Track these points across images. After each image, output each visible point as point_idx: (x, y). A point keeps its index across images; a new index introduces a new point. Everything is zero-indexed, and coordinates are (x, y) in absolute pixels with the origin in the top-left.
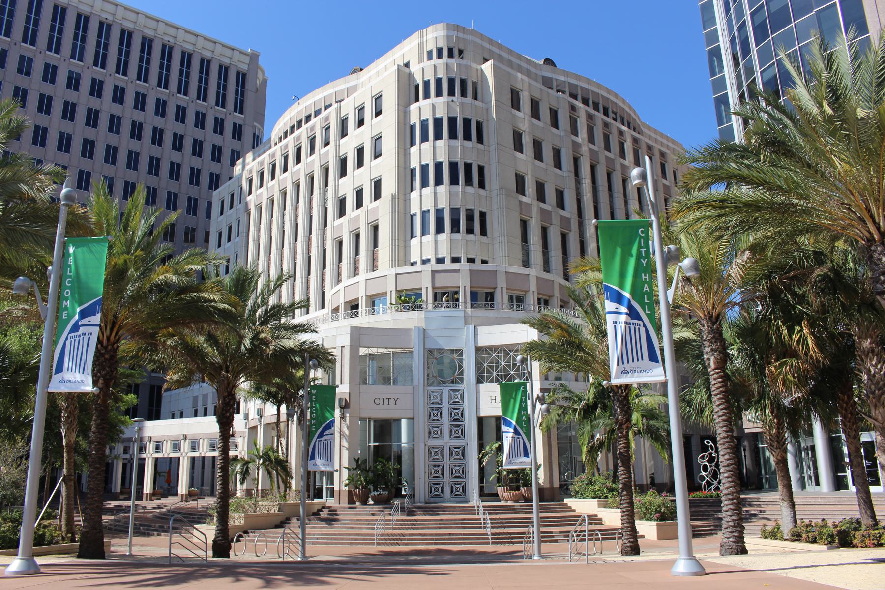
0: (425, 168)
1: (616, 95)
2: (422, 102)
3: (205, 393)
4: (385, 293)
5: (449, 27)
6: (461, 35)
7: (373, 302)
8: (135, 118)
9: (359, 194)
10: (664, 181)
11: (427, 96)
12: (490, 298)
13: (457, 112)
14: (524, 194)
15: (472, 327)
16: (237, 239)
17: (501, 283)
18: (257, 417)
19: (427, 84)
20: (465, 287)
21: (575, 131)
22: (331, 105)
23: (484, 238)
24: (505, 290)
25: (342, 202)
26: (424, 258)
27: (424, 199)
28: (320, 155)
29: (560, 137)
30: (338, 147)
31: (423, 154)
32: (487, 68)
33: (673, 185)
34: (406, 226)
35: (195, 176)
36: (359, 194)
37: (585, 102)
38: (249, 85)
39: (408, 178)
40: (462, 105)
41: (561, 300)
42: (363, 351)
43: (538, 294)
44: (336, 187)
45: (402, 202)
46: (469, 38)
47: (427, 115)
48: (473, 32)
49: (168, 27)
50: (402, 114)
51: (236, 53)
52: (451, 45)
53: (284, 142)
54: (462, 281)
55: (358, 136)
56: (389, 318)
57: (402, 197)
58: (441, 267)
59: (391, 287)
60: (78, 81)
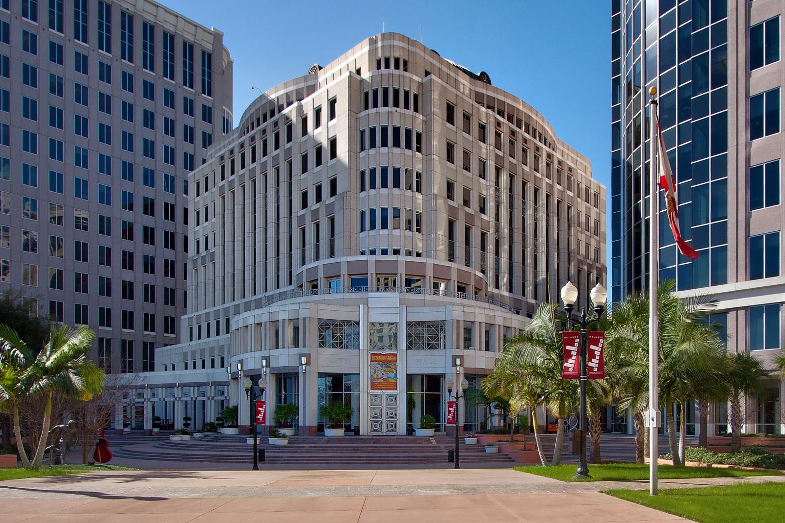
2: (372, 111)
7: (330, 283)
16: (214, 220)
35: (170, 155)
37: (510, 119)
41: (476, 288)
59: (344, 271)
60: (61, 86)
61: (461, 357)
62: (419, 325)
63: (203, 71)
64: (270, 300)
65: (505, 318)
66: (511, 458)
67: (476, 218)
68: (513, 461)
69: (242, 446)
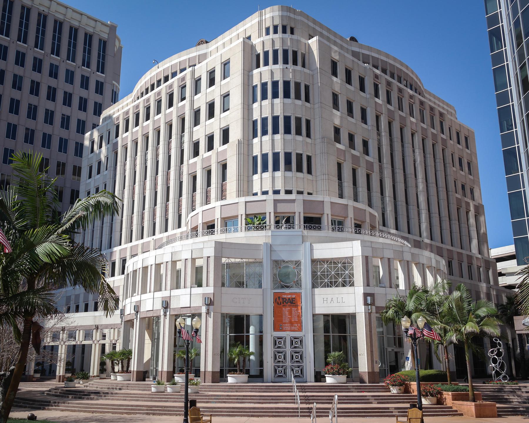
0: (264, 120)
1: (407, 67)
2: (262, 68)
3: (77, 293)
4: (237, 216)
5: (284, 9)
6: (292, 15)
7: (226, 223)
8: (16, 72)
9: (210, 139)
10: (442, 135)
11: (266, 64)
12: (289, 221)
13: (290, 77)
14: (339, 142)
15: (308, 244)
16: (106, 172)
17: (327, 210)
18: (133, 312)
19: (266, 54)
20: (300, 213)
21: (377, 95)
22: (185, 69)
23: (309, 176)
24: (330, 216)
25: (196, 145)
26: (263, 190)
27: (263, 145)
28: (178, 108)
29: (361, 99)
30: (192, 102)
31: (262, 109)
32: (313, 43)
33: (449, 138)
34: (253, 165)
36: (210, 139)
37: (384, 71)
38: (109, 51)
39: (253, 129)
40: (294, 71)
42: (224, 260)
43: (355, 219)
44: (191, 133)
45: (246, 146)
46: (299, 18)
47: (266, 78)
48: (301, 14)
49: (75, 14)
50: (246, 77)
51: (99, 24)
52: (285, 24)
53: (145, 97)
54: (298, 210)
55: (214, 93)
56: (240, 236)
57: (246, 142)
58: (277, 197)
59: (241, 211)
61: (372, 295)
62: (324, 262)
63: (99, 54)
64: (170, 240)
65: (413, 254)
66: (456, 411)
67: (361, 159)
68: (461, 415)
69: (146, 394)
